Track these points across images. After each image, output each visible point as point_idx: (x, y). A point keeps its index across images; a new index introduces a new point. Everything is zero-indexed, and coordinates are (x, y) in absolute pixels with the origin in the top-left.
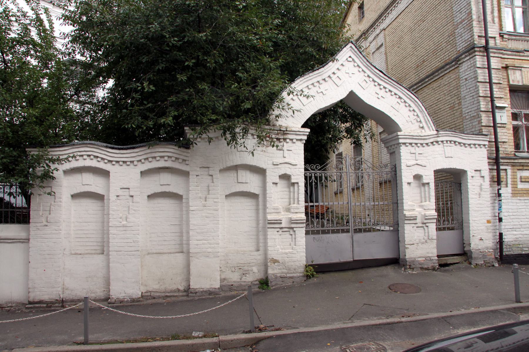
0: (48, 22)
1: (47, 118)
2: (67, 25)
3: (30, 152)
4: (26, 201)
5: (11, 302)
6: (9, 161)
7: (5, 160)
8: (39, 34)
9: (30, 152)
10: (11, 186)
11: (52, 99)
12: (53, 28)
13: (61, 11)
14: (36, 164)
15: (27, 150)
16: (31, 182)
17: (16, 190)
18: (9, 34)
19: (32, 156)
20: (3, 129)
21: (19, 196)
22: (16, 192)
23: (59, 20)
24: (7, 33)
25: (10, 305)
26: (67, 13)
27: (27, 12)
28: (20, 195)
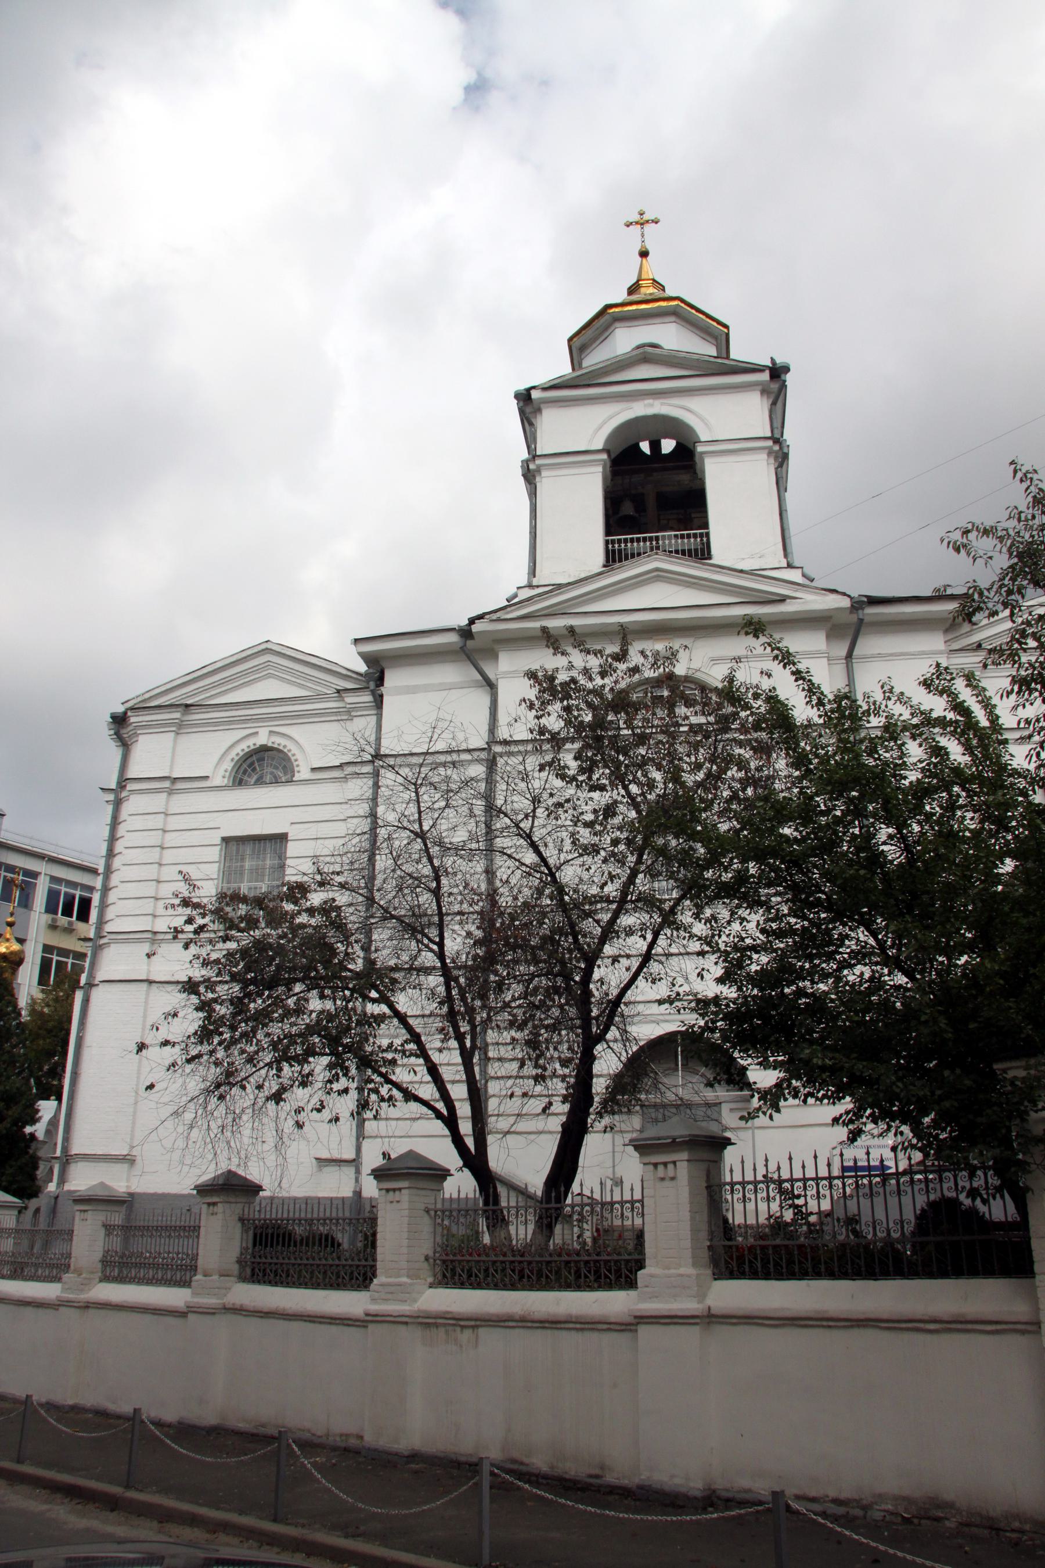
0: (980, 706)
1: (1032, 971)
2: (1027, 704)
3: (1005, 1071)
4: (1017, 1208)
5: (1017, 1517)
6: (956, 1104)
7: (947, 1104)
8: (968, 749)
9: (1005, 1071)
10: (972, 1175)
11: (1035, 915)
12: (998, 717)
13: (1008, 670)
14: (1026, 1103)
15: (995, 1066)
16: (1020, 1156)
17: (986, 1182)
18: (905, 778)
19: (1012, 1084)
20: (931, 1024)
21: (994, 1198)
22: (987, 1188)
23: (1008, 697)
24: (900, 775)
25: (1016, 1524)
26: (1023, 673)
27: (932, 710)
28: (998, 1196)
